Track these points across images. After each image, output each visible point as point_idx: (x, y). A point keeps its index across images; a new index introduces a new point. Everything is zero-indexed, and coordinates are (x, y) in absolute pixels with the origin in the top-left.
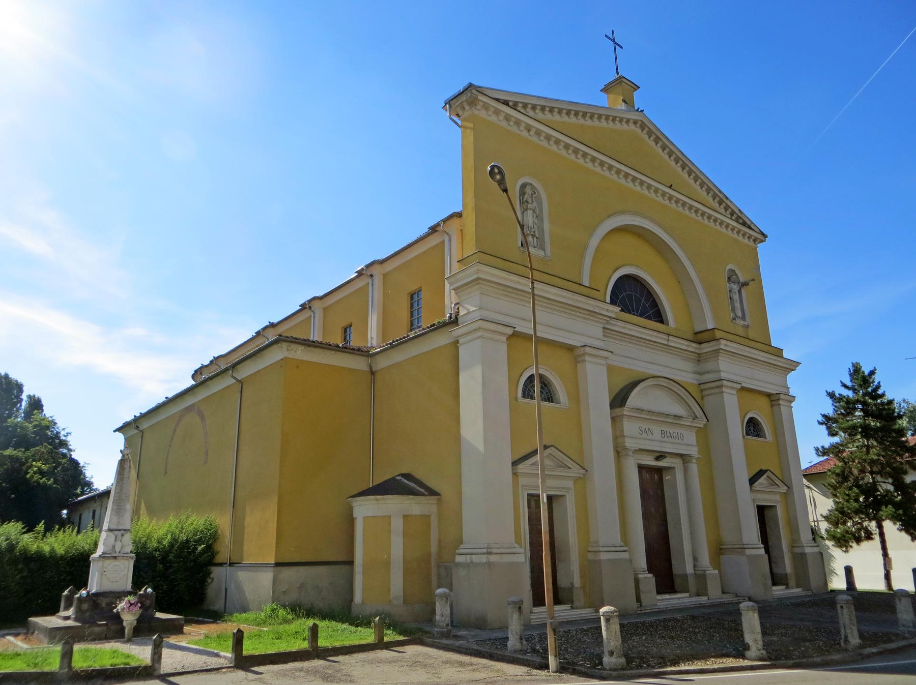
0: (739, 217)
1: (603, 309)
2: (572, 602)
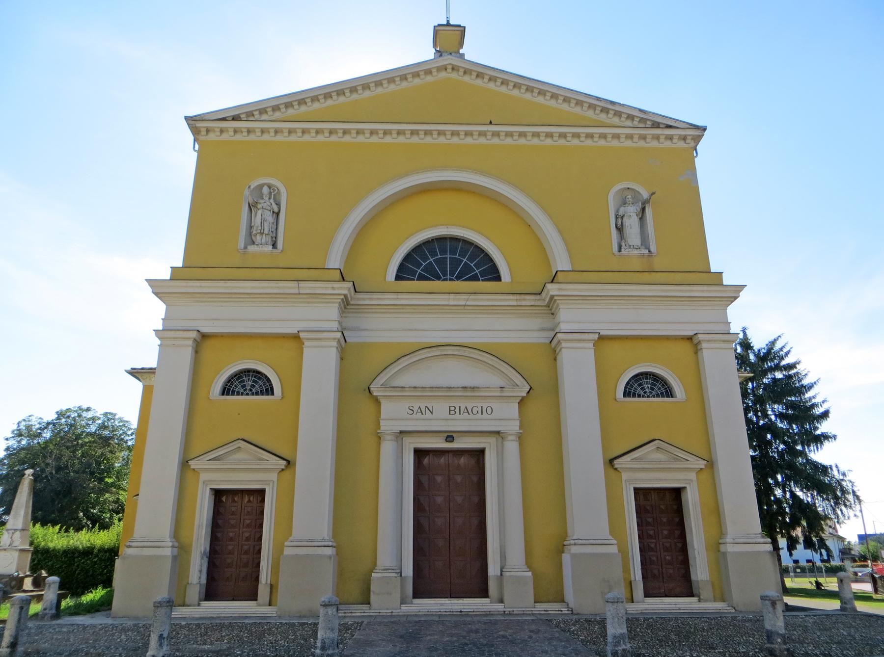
0: (642, 120)
1: (338, 288)
2: (699, 596)
